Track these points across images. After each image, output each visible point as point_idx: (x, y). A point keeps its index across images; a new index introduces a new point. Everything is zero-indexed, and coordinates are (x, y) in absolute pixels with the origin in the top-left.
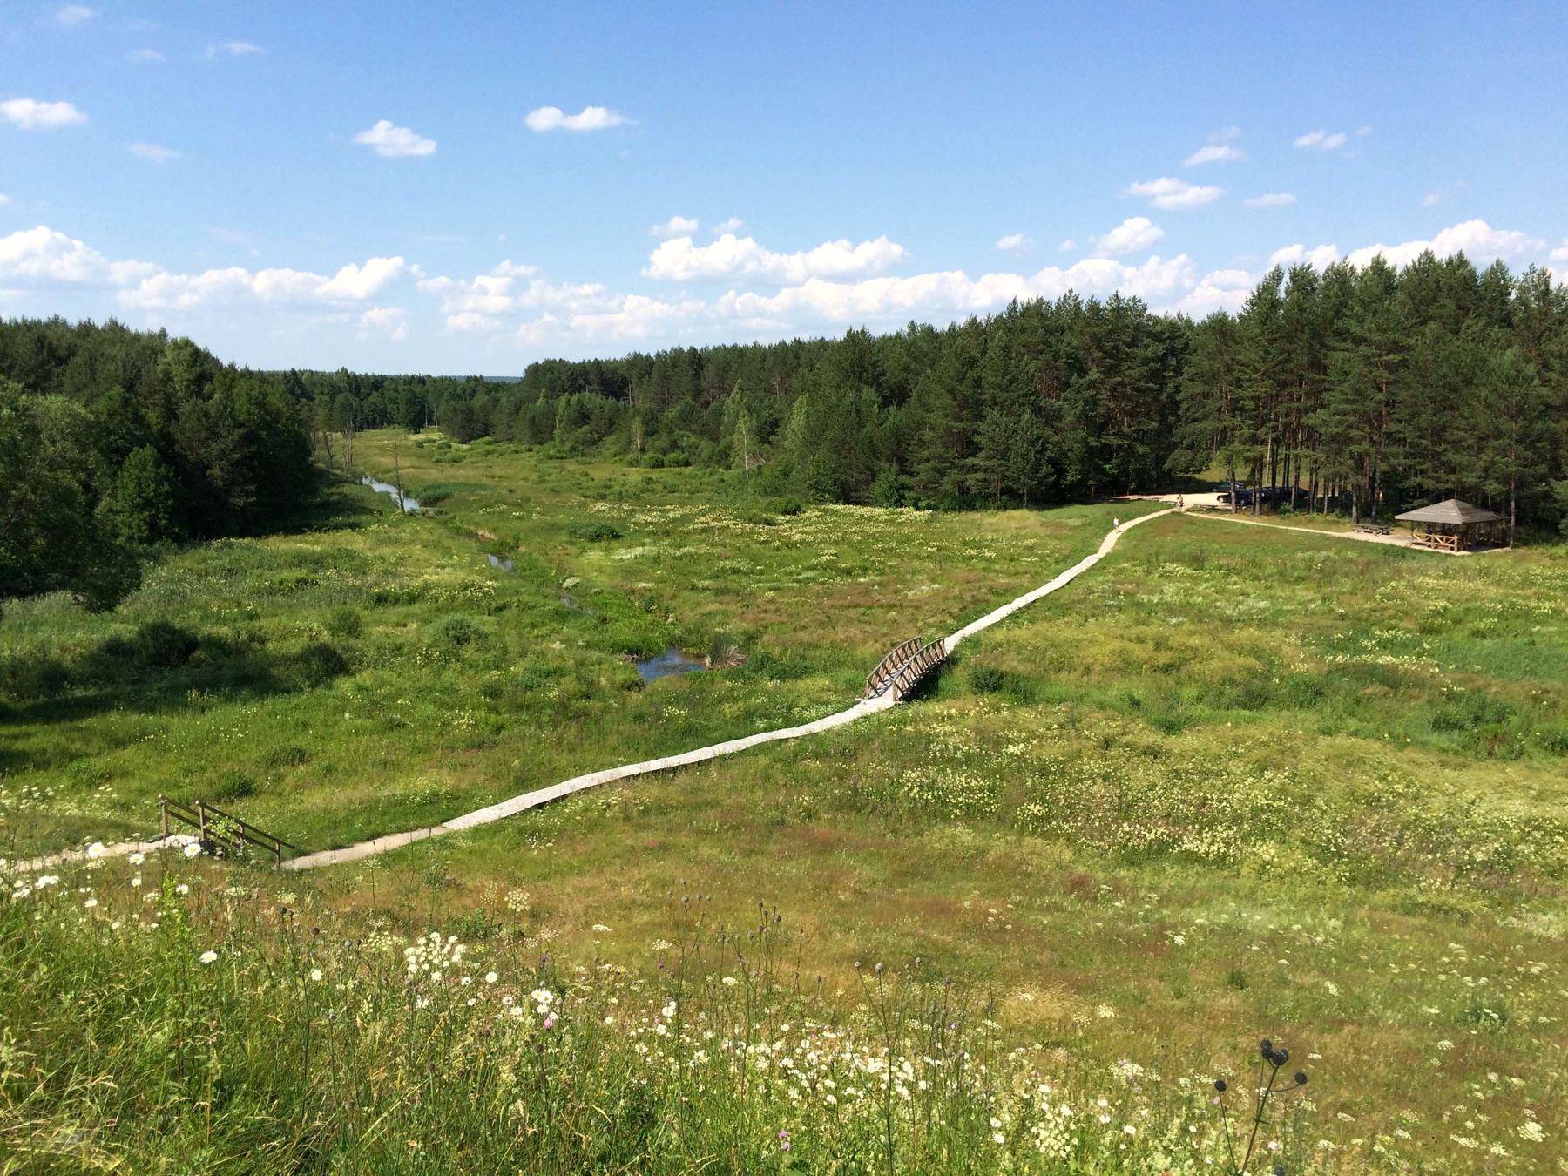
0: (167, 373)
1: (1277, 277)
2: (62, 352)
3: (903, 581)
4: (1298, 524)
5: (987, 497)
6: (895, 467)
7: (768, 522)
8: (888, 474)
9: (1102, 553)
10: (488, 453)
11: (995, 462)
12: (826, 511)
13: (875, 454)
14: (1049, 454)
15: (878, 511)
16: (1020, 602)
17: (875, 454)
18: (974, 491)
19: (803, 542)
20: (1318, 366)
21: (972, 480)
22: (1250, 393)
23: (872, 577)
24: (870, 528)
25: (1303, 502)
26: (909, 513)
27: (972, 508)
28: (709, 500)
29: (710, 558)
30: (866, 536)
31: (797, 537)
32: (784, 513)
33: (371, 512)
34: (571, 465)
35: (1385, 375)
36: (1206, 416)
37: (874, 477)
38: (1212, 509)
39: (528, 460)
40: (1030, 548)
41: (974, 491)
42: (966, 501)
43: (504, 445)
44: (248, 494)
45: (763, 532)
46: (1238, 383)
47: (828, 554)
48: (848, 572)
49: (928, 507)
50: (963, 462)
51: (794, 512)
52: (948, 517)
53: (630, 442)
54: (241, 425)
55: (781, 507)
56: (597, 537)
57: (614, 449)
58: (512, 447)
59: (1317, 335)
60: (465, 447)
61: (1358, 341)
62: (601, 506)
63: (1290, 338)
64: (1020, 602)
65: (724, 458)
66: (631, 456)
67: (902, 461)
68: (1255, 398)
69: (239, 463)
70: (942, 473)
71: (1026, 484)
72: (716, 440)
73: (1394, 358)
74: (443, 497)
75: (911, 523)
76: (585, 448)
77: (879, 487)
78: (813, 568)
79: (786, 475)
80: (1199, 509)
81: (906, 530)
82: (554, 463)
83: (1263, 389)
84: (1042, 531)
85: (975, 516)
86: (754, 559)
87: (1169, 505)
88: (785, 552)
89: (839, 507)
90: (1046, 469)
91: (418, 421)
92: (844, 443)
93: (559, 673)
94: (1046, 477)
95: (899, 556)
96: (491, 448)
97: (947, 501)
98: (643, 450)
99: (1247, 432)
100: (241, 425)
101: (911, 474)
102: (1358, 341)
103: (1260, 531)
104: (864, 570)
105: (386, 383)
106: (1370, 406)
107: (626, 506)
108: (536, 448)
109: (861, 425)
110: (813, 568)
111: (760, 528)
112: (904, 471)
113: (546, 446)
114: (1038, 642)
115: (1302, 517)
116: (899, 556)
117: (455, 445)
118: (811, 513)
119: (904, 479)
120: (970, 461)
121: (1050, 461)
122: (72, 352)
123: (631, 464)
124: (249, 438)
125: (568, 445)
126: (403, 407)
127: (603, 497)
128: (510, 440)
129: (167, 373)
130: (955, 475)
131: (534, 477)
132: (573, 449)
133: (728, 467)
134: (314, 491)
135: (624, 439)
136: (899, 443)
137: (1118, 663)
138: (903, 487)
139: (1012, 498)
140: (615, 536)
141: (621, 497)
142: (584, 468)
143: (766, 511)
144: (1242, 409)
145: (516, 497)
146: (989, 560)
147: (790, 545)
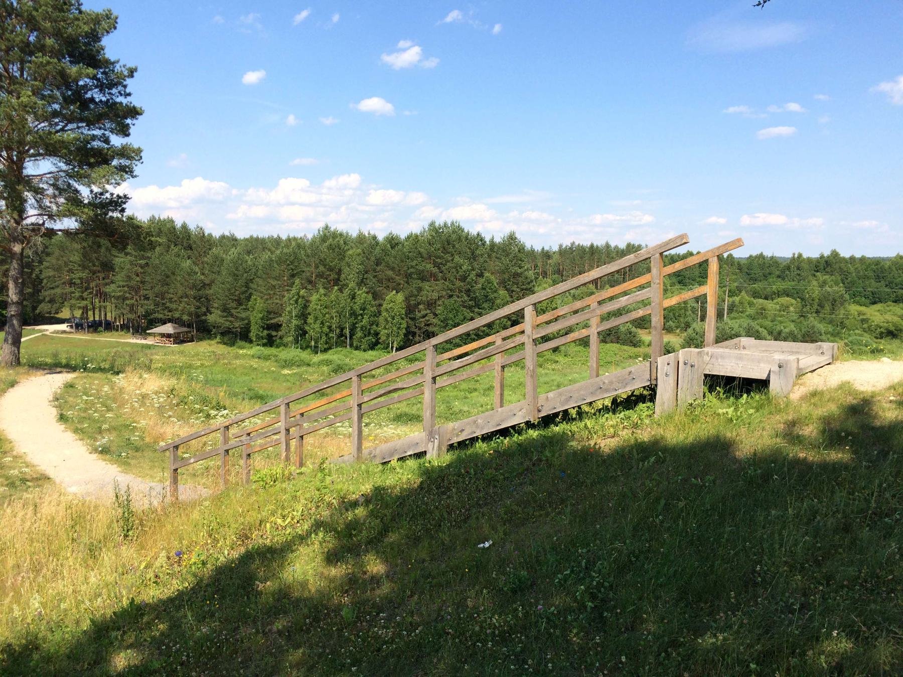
16: (595, 274)
25: (109, 327)
35: (140, 270)
38: (64, 332)
64: (595, 274)
68: (80, 279)
80: (57, 332)
87: (40, 331)
99: (77, 294)
106: (133, 283)
144: (74, 283)
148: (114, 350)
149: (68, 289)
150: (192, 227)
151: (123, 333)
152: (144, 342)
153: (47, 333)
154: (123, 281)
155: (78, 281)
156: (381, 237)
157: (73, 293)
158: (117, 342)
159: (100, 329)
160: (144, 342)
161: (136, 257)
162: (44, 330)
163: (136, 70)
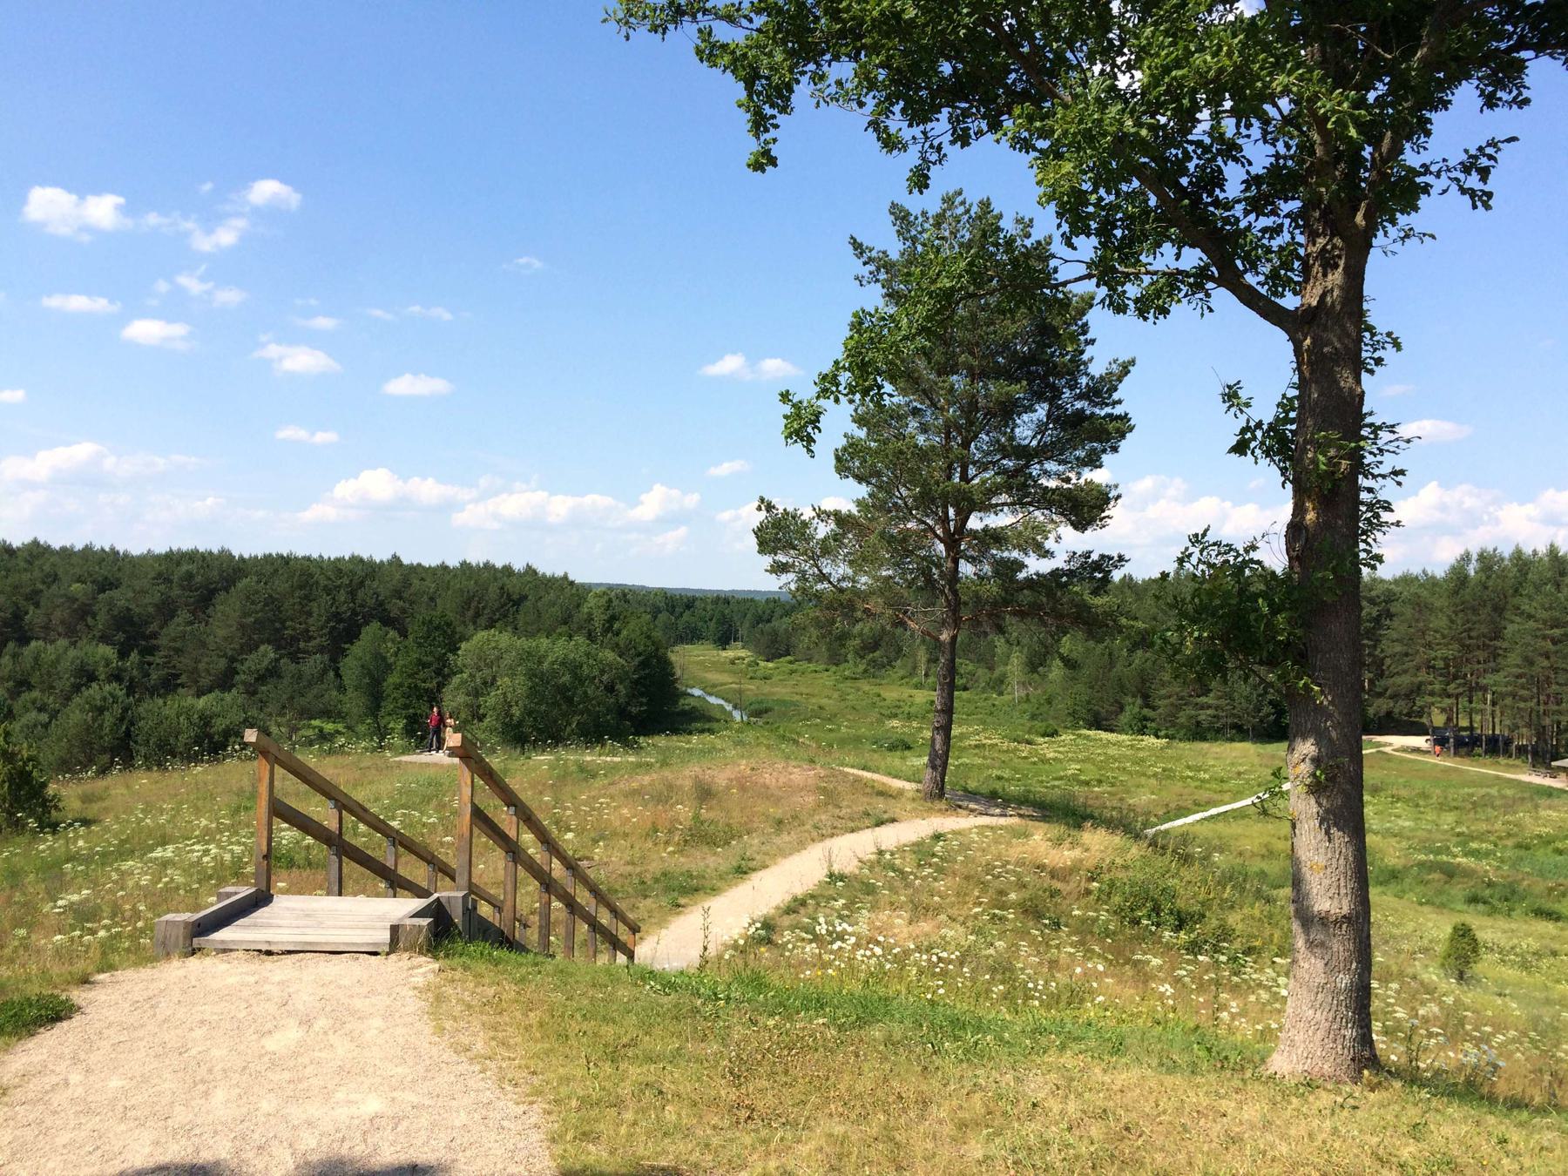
0: (590, 614)
1: (1466, 558)
2: (515, 597)
3: (1128, 792)
4: (1484, 766)
5: (1218, 731)
6: (1139, 701)
7: (1029, 742)
8: (1133, 707)
9: (721, 702)
10: (792, 672)
11: (1222, 702)
12: (1079, 736)
13: (1122, 689)
14: (1269, 697)
15: (1124, 737)
16: (1214, 811)
17: (1122, 689)
18: (1205, 725)
19: (1055, 759)
20: (1497, 634)
21: (1203, 716)
22: (1439, 654)
23: (1105, 788)
24: (1112, 751)
25: (1496, 747)
26: (1150, 740)
27: (1204, 739)
28: (984, 722)
29: (980, 767)
30: (1109, 758)
31: (1052, 755)
32: (1043, 736)
33: (718, 721)
34: (865, 686)
35: (1549, 645)
36: (1405, 672)
37: (1122, 709)
38: (1417, 750)
39: (827, 679)
40: (1239, 774)
41: (1205, 725)
42: (1199, 733)
43: (805, 665)
44: (642, 704)
45: (1025, 750)
46: (1429, 645)
47: (1073, 768)
48: (1087, 783)
49: (1166, 736)
50: (1199, 700)
51: (1052, 735)
52: (1182, 745)
53: (915, 668)
54: (639, 655)
55: (1042, 730)
56: (892, 748)
57: (902, 673)
58: (812, 666)
59: (1499, 609)
60: (770, 665)
61: (1530, 617)
62: (895, 723)
63: (1475, 611)
64: (1214, 811)
65: (998, 684)
66: (915, 680)
67: (1146, 697)
68: (1445, 659)
69: (637, 682)
70: (1179, 708)
71: (1249, 722)
72: (991, 669)
73: (1557, 632)
74: (766, 711)
75: (1150, 749)
76: (876, 669)
77: (1124, 718)
78: (1061, 778)
79: (1049, 702)
80: (1405, 749)
81: (1141, 754)
82: (849, 683)
83: (1451, 652)
84: (1256, 761)
85: (1205, 745)
86: (1016, 771)
87: (1379, 745)
88: (1041, 766)
89: (1091, 733)
90: (1267, 709)
91: (725, 639)
92: (1097, 680)
93: (933, 740)
94: (1268, 715)
95: (1130, 773)
96: (794, 667)
97: (1182, 732)
98: (926, 675)
99: (1437, 687)
100: (639, 655)
101: (1154, 709)
102: (1530, 617)
103: (1447, 770)
104: (1100, 782)
105: (697, 603)
106: (1536, 670)
107: (915, 724)
108: (834, 668)
109: (1112, 664)
110: (1061, 778)
111: (1022, 747)
112: (1148, 706)
113: (841, 667)
114: (1210, 835)
115: (1488, 760)
116: (1130, 773)
117: (762, 664)
118: (1066, 737)
119: (1146, 711)
120: (1203, 699)
121: (1271, 702)
122: (524, 598)
123: (916, 687)
124: (644, 664)
125: (862, 667)
126: (712, 625)
127: (895, 716)
128: (809, 660)
129: (590, 614)
130: (1190, 711)
131: (836, 695)
132: (865, 671)
133: (1001, 694)
134: (677, 702)
135: (910, 665)
136: (1143, 681)
137: (1264, 851)
138: (1145, 719)
139: (1240, 732)
140: (909, 748)
141: (909, 717)
142: (876, 690)
143: (1029, 732)
144: (1433, 667)
145: (825, 714)
146: (1203, 781)
147: (1044, 761)
148: (1483, 791)
149: (1423, 676)
150: (246, 556)
151: (1518, 762)
152: (1548, 782)
153: (1388, 750)
154: (1518, 666)
155: (1440, 664)
156: (430, 480)
157: (1431, 683)
158: (1498, 777)
159: (1478, 750)
160: (1548, 782)
161: (1545, 622)
162: (1385, 745)
163: (1132, 363)
